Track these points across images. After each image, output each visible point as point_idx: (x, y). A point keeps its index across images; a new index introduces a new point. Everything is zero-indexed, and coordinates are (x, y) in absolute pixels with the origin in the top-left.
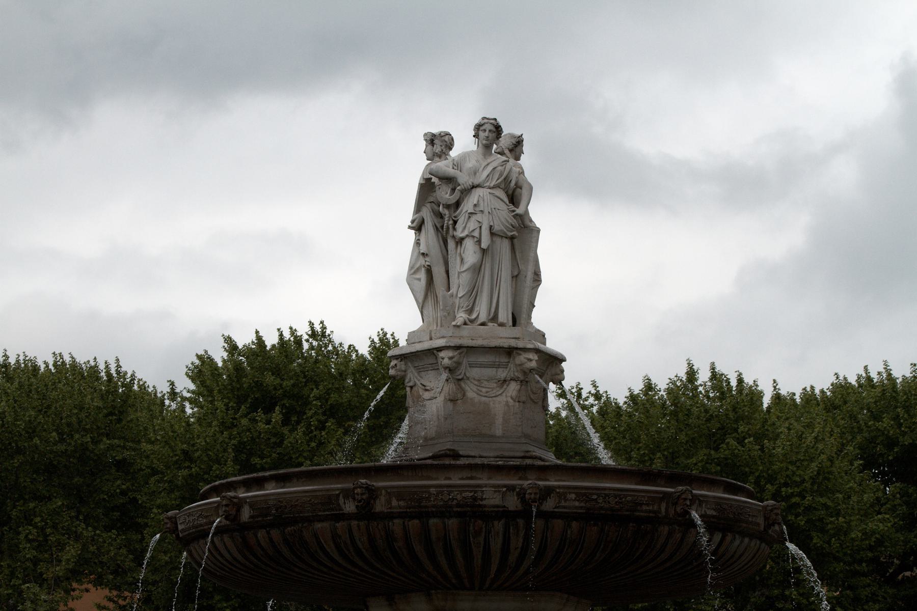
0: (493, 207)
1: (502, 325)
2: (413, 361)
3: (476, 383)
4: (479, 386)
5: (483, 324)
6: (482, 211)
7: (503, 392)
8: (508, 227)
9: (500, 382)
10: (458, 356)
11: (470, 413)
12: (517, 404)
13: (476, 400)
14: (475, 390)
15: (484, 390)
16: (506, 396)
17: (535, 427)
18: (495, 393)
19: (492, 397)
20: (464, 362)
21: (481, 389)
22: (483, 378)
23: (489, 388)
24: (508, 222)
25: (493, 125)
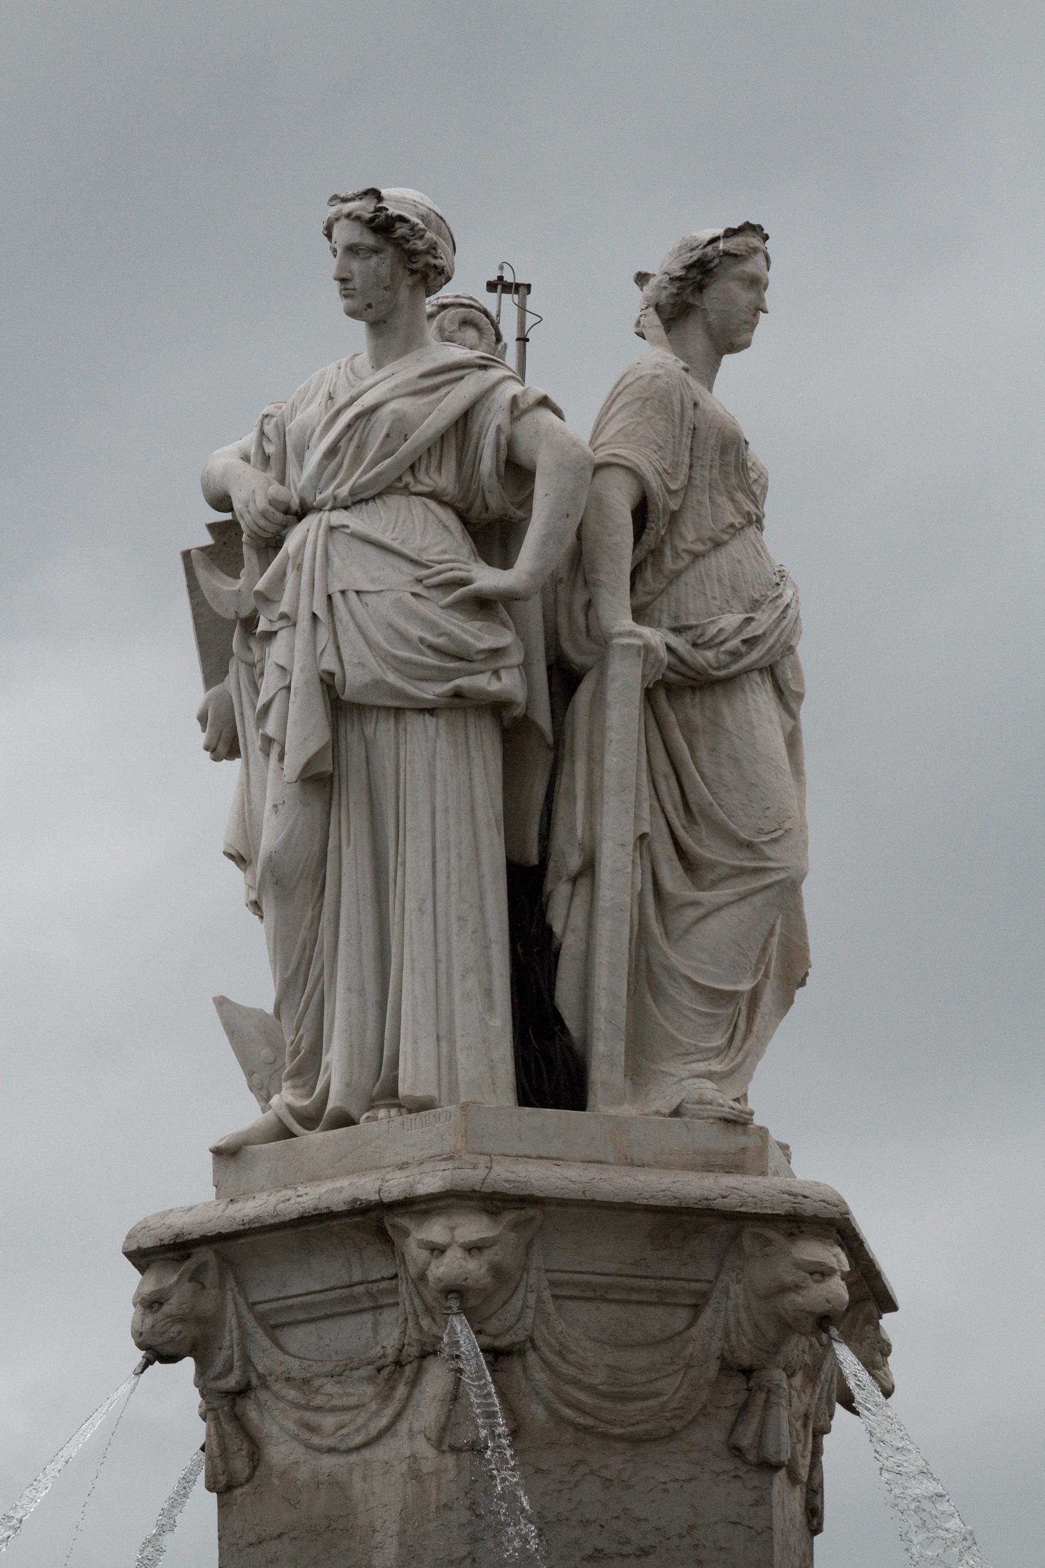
0: (335, 588)
1: (423, 1106)
2: (769, 1242)
3: (292, 1394)
4: (307, 1407)
5: (344, 1120)
6: (284, 616)
7: (398, 1415)
8: (407, 662)
9: (385, 1373)
10: (187, 1287)
11: (280, 1535)
12: (450, 1460)
13: (303, 1474)
14: (292, 1427)
15: (329, 1422)
16: (411, 1435)
17: (644, 1552)
18: (365, 1425)
19: (358, 1448)
20: (232, 1321)
21: (310, 1417)
22: (316, 1368)
23: (345, 1409)
24: (405, 639)
25: (358, 218)
